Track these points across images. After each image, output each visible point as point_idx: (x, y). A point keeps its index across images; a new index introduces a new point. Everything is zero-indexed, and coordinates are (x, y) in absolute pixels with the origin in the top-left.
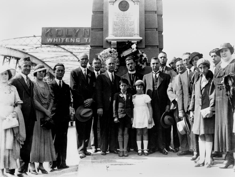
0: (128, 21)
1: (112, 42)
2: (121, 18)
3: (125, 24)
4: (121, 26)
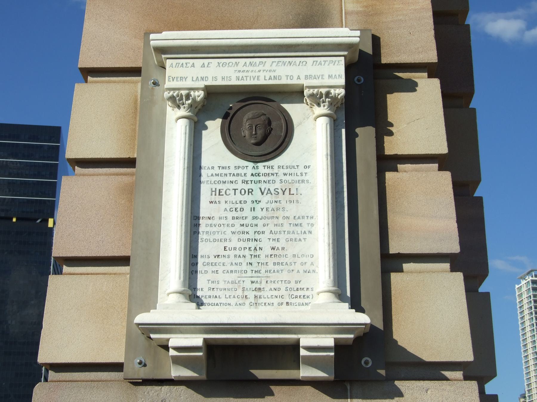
0: (281, 214)
1: (306, 340)
2: (239, 197)
3: (263, 233)
4: (239, 240)
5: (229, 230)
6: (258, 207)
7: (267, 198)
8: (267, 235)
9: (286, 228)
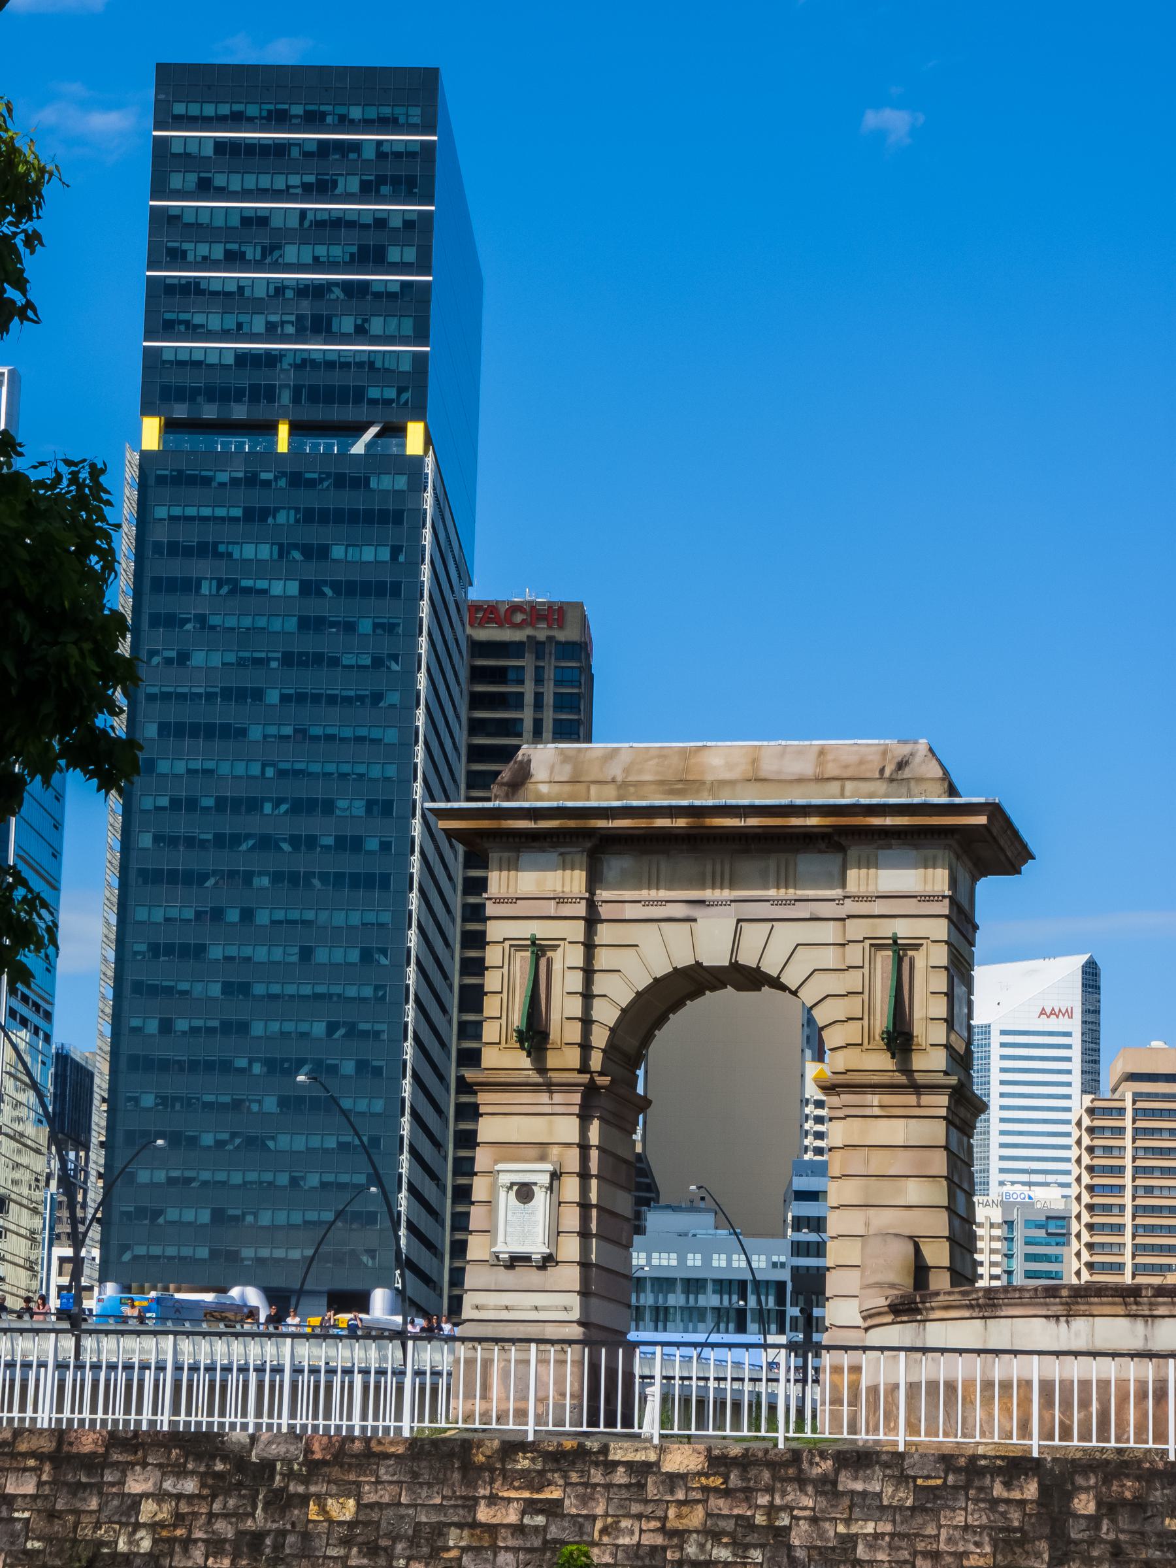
1: (533, 1256)
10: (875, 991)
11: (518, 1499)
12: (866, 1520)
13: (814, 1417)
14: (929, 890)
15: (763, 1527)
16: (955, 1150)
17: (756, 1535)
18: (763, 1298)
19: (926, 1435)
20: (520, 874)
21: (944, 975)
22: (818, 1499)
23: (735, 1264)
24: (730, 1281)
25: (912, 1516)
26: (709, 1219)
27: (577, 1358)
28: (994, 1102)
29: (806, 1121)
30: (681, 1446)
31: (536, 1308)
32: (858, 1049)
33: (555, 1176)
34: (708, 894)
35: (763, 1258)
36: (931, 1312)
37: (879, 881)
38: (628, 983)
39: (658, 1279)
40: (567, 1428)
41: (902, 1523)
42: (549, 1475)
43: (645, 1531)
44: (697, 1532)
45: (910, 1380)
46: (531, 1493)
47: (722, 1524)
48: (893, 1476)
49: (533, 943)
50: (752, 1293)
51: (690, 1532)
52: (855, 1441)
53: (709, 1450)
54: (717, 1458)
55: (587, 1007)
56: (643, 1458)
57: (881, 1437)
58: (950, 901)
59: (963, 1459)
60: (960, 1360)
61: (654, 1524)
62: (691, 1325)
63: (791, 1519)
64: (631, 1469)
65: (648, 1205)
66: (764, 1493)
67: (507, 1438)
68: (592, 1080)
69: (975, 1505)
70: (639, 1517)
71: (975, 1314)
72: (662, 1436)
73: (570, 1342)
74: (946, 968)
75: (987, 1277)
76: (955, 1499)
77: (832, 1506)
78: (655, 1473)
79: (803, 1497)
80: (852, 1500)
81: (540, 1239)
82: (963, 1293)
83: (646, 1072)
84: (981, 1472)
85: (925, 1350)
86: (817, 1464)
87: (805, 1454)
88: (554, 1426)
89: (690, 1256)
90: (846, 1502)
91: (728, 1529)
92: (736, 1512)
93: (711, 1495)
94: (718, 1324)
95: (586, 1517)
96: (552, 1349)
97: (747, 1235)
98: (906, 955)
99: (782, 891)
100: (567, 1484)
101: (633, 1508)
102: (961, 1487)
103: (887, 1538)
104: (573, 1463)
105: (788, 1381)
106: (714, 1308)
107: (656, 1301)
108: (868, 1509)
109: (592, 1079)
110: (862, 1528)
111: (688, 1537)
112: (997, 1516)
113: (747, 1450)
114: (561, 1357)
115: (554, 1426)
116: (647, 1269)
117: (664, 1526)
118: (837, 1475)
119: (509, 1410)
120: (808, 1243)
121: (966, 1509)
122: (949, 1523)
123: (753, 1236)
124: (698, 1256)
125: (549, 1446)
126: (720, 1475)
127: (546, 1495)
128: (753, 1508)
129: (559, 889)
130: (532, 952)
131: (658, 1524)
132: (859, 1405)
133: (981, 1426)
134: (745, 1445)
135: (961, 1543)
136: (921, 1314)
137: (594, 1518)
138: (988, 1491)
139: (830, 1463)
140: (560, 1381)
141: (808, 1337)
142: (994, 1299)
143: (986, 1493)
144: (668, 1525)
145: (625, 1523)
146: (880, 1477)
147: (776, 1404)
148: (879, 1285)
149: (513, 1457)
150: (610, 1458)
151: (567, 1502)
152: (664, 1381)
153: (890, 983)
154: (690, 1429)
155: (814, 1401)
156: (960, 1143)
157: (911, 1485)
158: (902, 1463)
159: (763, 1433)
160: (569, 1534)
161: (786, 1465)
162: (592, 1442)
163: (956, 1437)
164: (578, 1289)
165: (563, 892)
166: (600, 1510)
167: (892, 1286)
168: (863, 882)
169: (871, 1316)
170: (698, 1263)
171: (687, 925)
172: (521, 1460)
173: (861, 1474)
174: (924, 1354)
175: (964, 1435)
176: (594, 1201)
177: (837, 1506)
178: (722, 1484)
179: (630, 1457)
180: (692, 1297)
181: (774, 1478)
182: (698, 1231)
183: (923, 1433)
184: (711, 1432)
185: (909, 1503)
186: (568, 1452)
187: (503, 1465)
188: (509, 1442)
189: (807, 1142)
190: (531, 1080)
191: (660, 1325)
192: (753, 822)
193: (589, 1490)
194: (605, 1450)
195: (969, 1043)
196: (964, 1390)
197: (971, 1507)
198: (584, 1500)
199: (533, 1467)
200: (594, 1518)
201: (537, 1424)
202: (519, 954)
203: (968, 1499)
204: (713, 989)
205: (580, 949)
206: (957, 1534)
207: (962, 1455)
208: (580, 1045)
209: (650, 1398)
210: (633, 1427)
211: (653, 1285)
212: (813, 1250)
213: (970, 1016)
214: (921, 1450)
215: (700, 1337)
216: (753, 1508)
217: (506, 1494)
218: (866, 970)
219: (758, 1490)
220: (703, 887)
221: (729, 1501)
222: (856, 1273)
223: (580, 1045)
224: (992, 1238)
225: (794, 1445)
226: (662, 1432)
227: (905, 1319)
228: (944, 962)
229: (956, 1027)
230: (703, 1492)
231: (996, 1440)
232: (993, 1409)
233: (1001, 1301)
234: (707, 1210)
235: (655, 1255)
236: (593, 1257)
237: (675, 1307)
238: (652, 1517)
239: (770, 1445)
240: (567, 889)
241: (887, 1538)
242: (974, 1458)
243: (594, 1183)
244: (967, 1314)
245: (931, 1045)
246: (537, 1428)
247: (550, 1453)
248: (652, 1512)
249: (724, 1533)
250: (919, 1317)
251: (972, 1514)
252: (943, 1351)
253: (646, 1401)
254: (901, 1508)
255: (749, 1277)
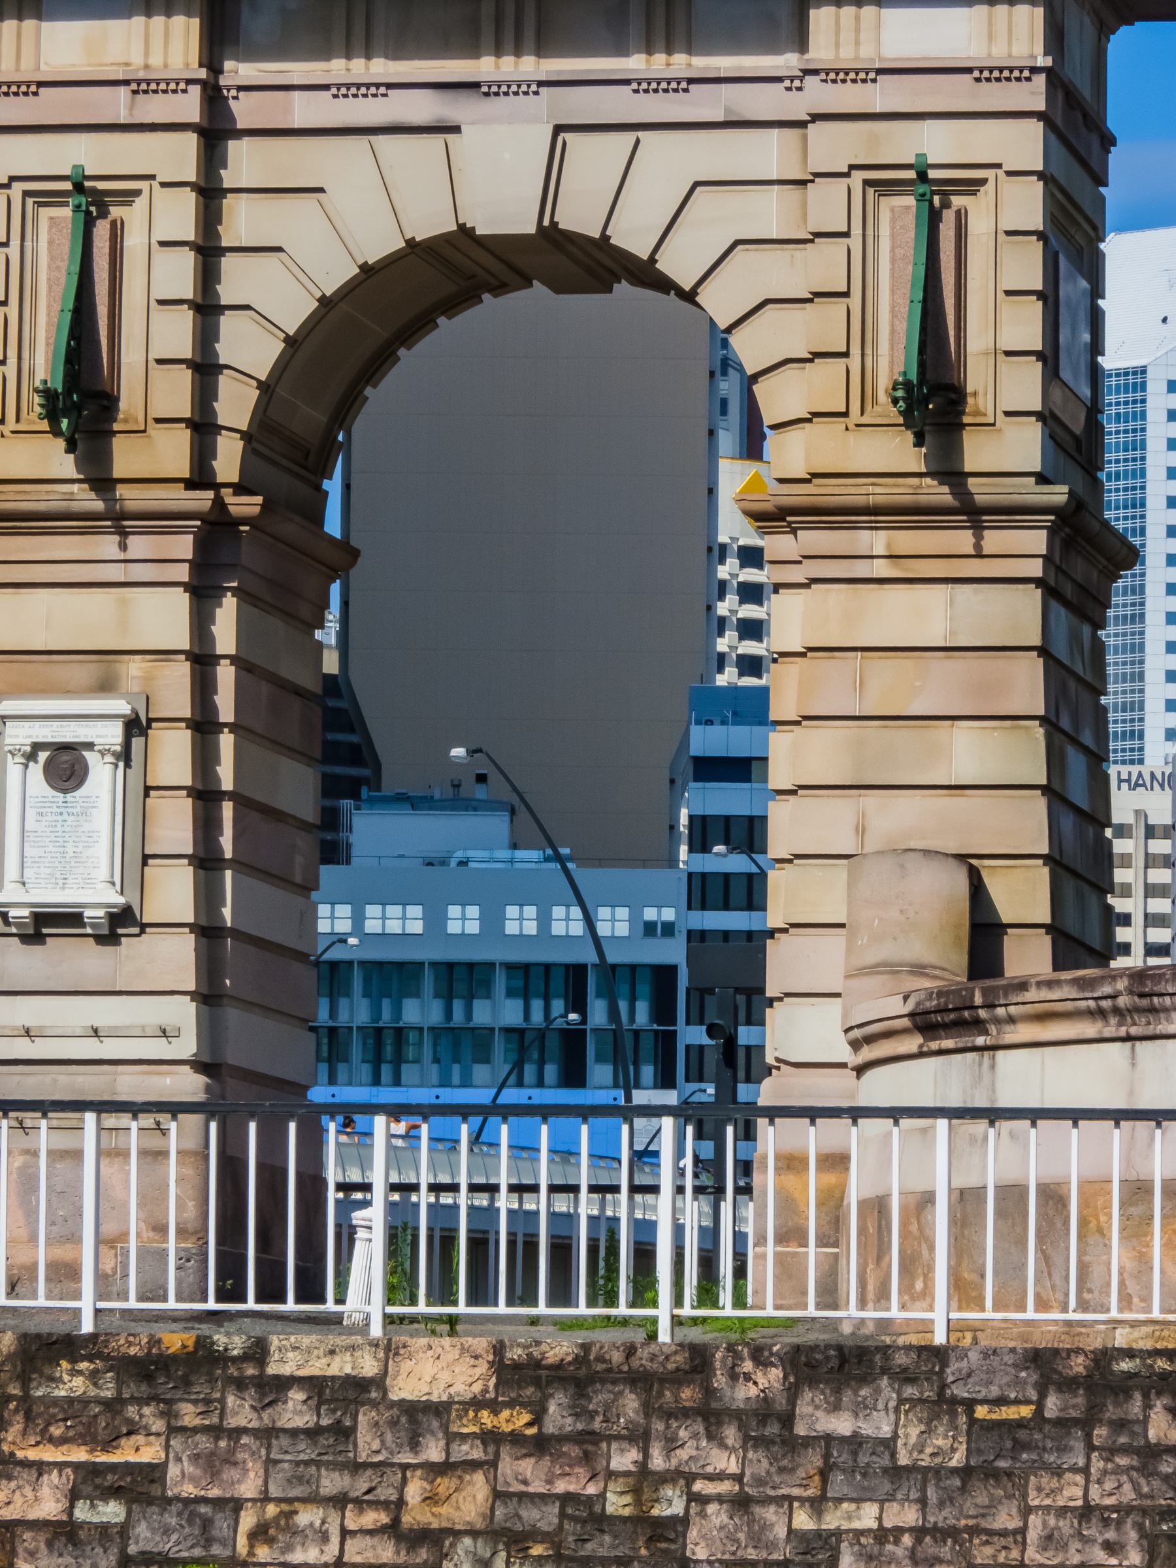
0: (80, 829)
1: (88, 913)
5: (47, 840)
6: (66, 824)
7: (72, 818)
8: (71, 843)
9: (83, 838)
10: (876, 288)
11: (61, 1466)
12: (858, 1501)
13: (740, 1272)
14: (999, 53)
15: (624, 1520)
16: (1064, 657)
17: (607, 1538)
18: (623, 1006)
19: (996, 1308)
20: (45, 25)
21: (1035, 249)
22: (750, 1455)
23: (558, 929)
24: (547, 967)
25: (963, 1489)
26: (497, 825)
27: (192, 1144)
28: (1156, 547)
29: (721, 596)
30: (435, 1342)
31: (96, 1032)
32: (839, 424)
33: (135, 727)
34: (485, 67)
35: (623, 913)
36: (1008, 1028)
37: (885, 36)
38: (300, 273)
39: (380, 965)
40: (172, 1304)
41: (941, 1504)
42: (131, 1411)
43: (353, 1533)
44: (474, 1533)
45: (958, 1183)
46: (92, 1451)
47: (531, 1515)
48: (921, 1401)
49: (79, 188)
50: (599, 995)
51: (457, 1534)
52: (834, 1324)
53: (499, 1349)
54: (517, 1366)
55: (206, 336)
56: (348, 1370)
57: (894, 1312)
58: (1050, 83)
59: (1081, 1359)
60: (1073, 1136)
61: (373, 1518)
62: (456, 1068)
63: (689, 1501)
64: (320, 1394)
65: (356, 796)
66: (625, 1445)
67: (32, 1327)
68: (219, 504)
69: (1107, 1460)
70: (340, 1501)
71: (1109, 1031)
72: (390, 1320)
73: (175, 1109)
74: (1041, 235)
75: (1138, 949)
76: (1063, 1449)
77: (781, 1470)
78: (374, 1404)
79: (715, 1452)
80: (827, 1456)
81: (103, 873)
82: (1080, 983)
83: (347, 487)
84: (1122, 1387)
85: (993, 1115)
86: (748, 1377)
87: (719, 1355)
88: (140, 1299)
89: (454, 911)
90: (813, 1460)
91: (543, 1526)
92: (561, 1487)
93: (505, 1451)
94: (518, 1066)
95: (218, 1503)
96: (134, 1125)
97: (583, 862)
98: (946, 205)
99: (660, 58)
100: (173, 1430)
101: (325, 1482)
102: (1076, 1422)
103: (907, 1540)
104: (186, 1383)
105: (680, 1190)
106: (508, 1030)
107: (377, 1013)
108: (864, 1475)
109: (219, 503)
110: (849, 1518)
111: (453, 1545)
112: (1156, 1483)
113: (586, 1347)
114: (155, 1142)
115: (140, 1299)
116: (352, 941)
117: (396, 1521)
118: (792, 1402)
119: (35, 1265)
120: (727, 876)
121: (1086, 1471)
122: (1048, 1502)
123: (600, 862)
124: (473, 911)
125: (130, 1344)
126: (523, 1405)
127: (127, 1453)
128: (601, 1477)
129: (137, 60)
130: (77, 207)
131: (384, 1518)
132: (843, 1242)
133: (1122, 1284)
134: (581, 1337)
135: (1075, 1545)
136: (986, 1033)
137: (236, 1505)
138: (1137, 1428)
139: (776, 1373)
140: (153, 1197)
141: (727, 1094)
142: (1151, 995)
143: (1133, 1434)
144: (407, 1519)
145: (307, 1517)
146: (892, 1404)
147: (654, 1245)
148: (889, 968)
149: (47, 1371)
150: (272, 1370)
151: (173, 1471)
152: (396, 1197)
153: (912, 271)
154: (455, 1303)
155: (739, 1238)
156: (1074, 638)
157: (962, 1419)
158: (942, 1371)
159: (622, 1309)
160: (178, 1543)
161: (677, 1379)
162: (228, 1334)
163: (1065, 1309)
164: (192, 987)
165: (147, 67)
166: (248, 1488)
167: (919, 970)
168: (847, 36)
169: (869, 1040)
170: (473, 928)
171: (436, 142)
172: (66, 1378)
173: (847, 1397)
174: (992, 1123)
175: (1083, 1306)
176: (227, 784)
177: (792, 1470)
178: (530, 1424)
179: (317, 1367)
180: (458, 1006)
181: (647, 1409)
182: (471, 854)
183: (989, 1303)
184: (502, 1309)
185: (957, 1460)
186: (174, 1358)
187: (25, 1387)
188: (38, 1336)
189: (722, 645)
190: (76, 506)
191: (386, 1070)
192: (951, 333)
193: (223, 1444)
194: (258, 1352)
195: (1094, 409)
196: (1084, 1203)
197: (1097, 1464)
198: (212, 1465)
199: (93, 1392)
200: (236, 1505)
201: (100, 1296)
202: (46, 213)
203: (1090, 1448)
204: (500, 288)
205: (188, 200)
206: (1066, 1526)
207: (1078, 1351)
208: (189, 423)
209: (361, 1234)
210: (322, 1299)
211: (367, 980)
212: (738, 892)
213: (1097, 347)
214: (984, 1342)
215: (481, 1096)
216: (601, 1477)
217: (32, 1455)
218: (855, 242)
219: (610, 1439)
220: (474, 52)
221: (546, 1461)
222: (835, 942)
223: (189, 423)
224: (1151, 861)
225: (695, 1335)
226: (390, 1310)
227: (949, 1044)
228: (1035, 220)
229: (1065, 374)
230: (484, 1443)
231: (1156, 1314)
232: (1149, 1245)
233: (1167, 1000)
234: (490, 806)
235: (372, 910)
236: (227, 912)
237: (421, 1029)
238: (369, 1502)
239: (639, 1336)
240: (156, 60)
241: (907, 1540)
242: (1104, 1357)
243: (226, 742)
244: (1089, 1029)
245: (1008, 414)
246: (101, 1305)
247: (134, 1360)
248: (369, 1492)
249: (533, 1535)
250: (980, 1041)
251: (1099, 1482)
252: (1035, 1115)
253: (352, 1241)
254: (938, 1472)
255: (591, 957)
